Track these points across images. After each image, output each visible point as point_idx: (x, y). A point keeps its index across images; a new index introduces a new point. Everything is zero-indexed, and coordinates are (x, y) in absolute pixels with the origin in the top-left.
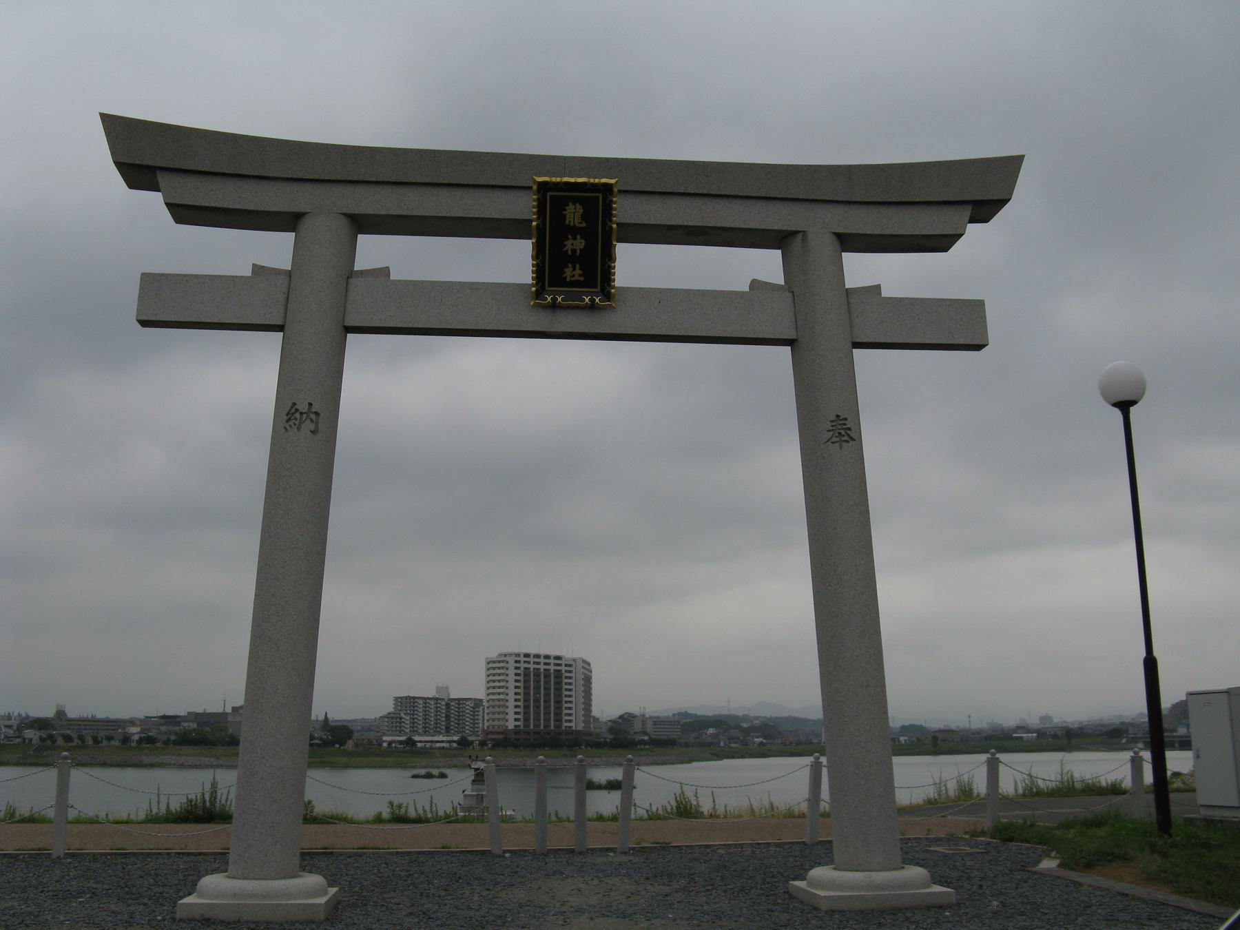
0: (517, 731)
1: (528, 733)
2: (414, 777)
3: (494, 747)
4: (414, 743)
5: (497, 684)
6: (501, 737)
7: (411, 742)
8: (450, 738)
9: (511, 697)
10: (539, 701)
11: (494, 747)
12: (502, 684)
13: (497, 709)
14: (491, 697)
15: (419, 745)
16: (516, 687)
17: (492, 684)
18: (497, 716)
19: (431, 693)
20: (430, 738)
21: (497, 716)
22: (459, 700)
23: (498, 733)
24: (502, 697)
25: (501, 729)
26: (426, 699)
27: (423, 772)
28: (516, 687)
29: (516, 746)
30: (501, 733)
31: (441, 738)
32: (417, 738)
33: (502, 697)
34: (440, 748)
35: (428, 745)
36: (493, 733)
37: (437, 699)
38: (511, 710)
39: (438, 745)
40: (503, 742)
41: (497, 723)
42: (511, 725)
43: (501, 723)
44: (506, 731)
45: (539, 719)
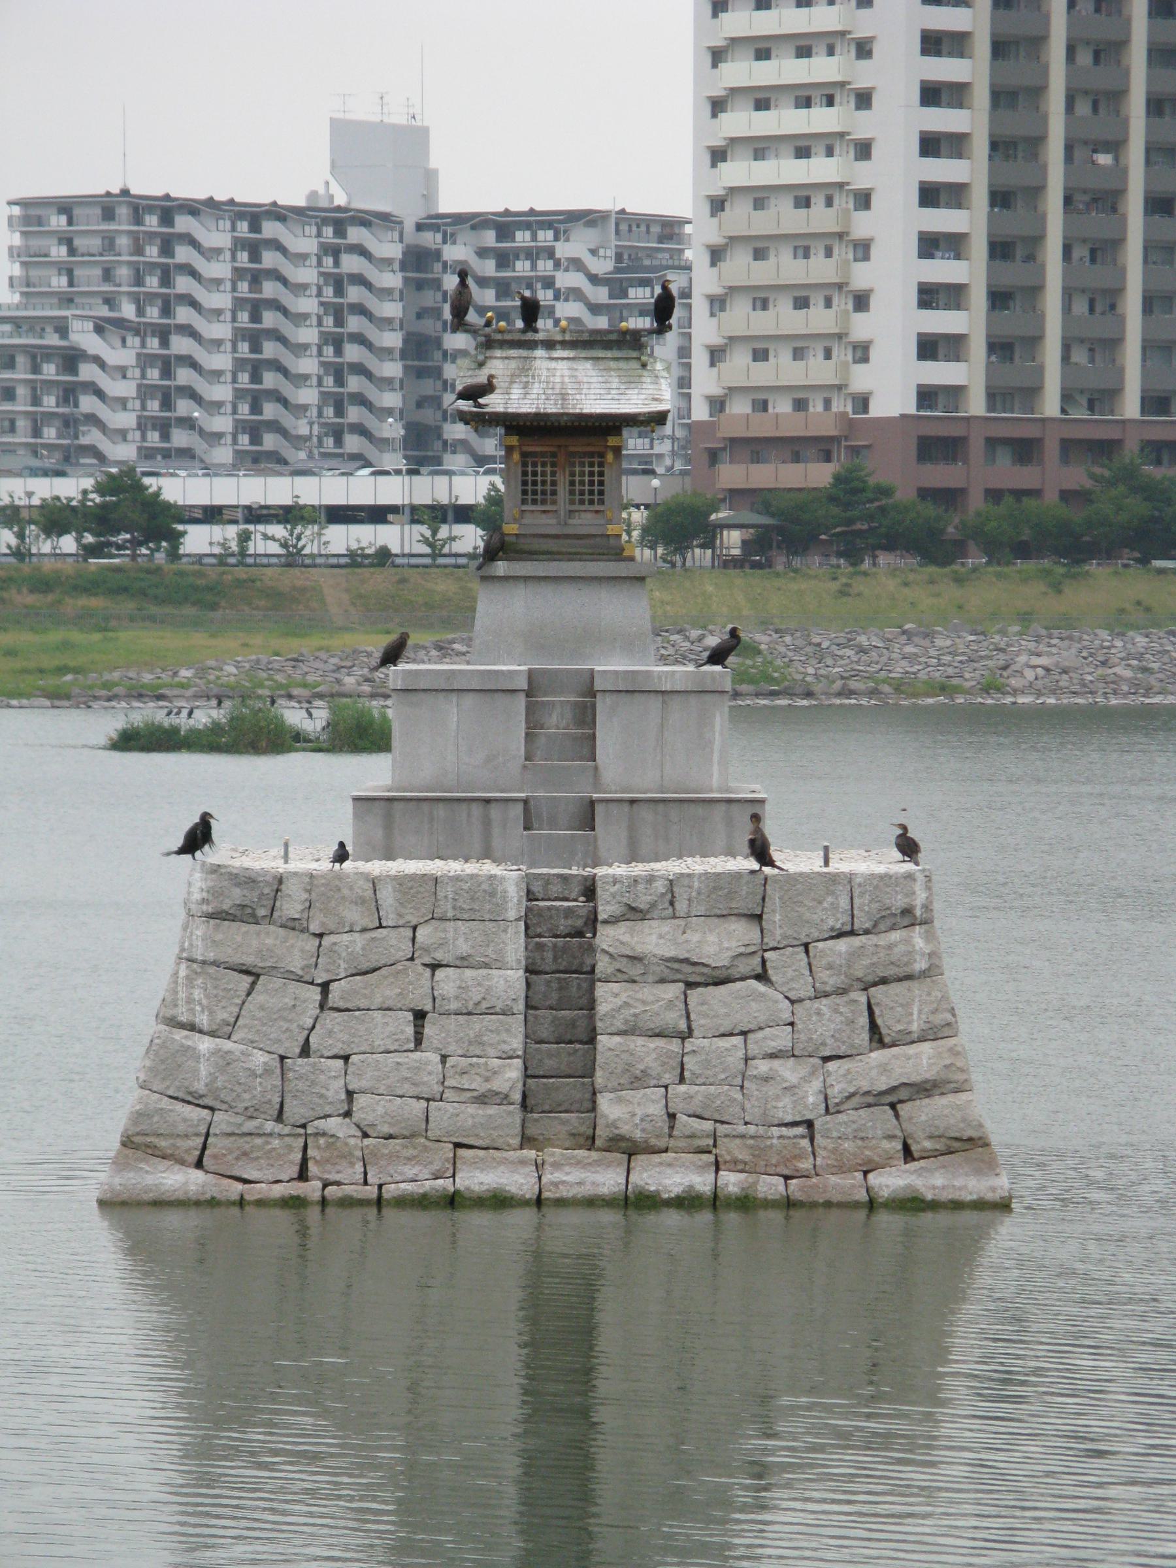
0: (936, 436)
1: (1025, 450)
2: (128, 741)
3: (760, 552)
4: (161, 523)
5: (786, 70)
6: (819, 475)
7: (130, 515)
8: (427, 489)
9: (896, 172)
10: (1108, 200)
11: (760, 552)
12: (822, 69)
13: (785, 268)
14: (740, 172)
15: (198, 540)
16: (930, 296)
17: (742, 72)
18: (784, 318)
19: (292, 174)
20: (277, 490)
21: (784, 318)
22: (505, 224)
23: (795, 448)
24: (821, 169)
25: (819, 421)
26: (255, 215)
27: (515, 867)
28: (931, 245)
29: (928, 540)
30: (824, 448)
31: (362, 489)
32: (178, 488)
33: (821, 169)
34: (354, 559)
35: (268, 541)
36: (755, 448)
37: (340, 220)
38: (893, 272)
39: (340, 539)
40: (841, 509)
41: (783, 370)
42: (891, 386)
43: (817, 370)
44: (848, 438)
45: (1108, 346)
